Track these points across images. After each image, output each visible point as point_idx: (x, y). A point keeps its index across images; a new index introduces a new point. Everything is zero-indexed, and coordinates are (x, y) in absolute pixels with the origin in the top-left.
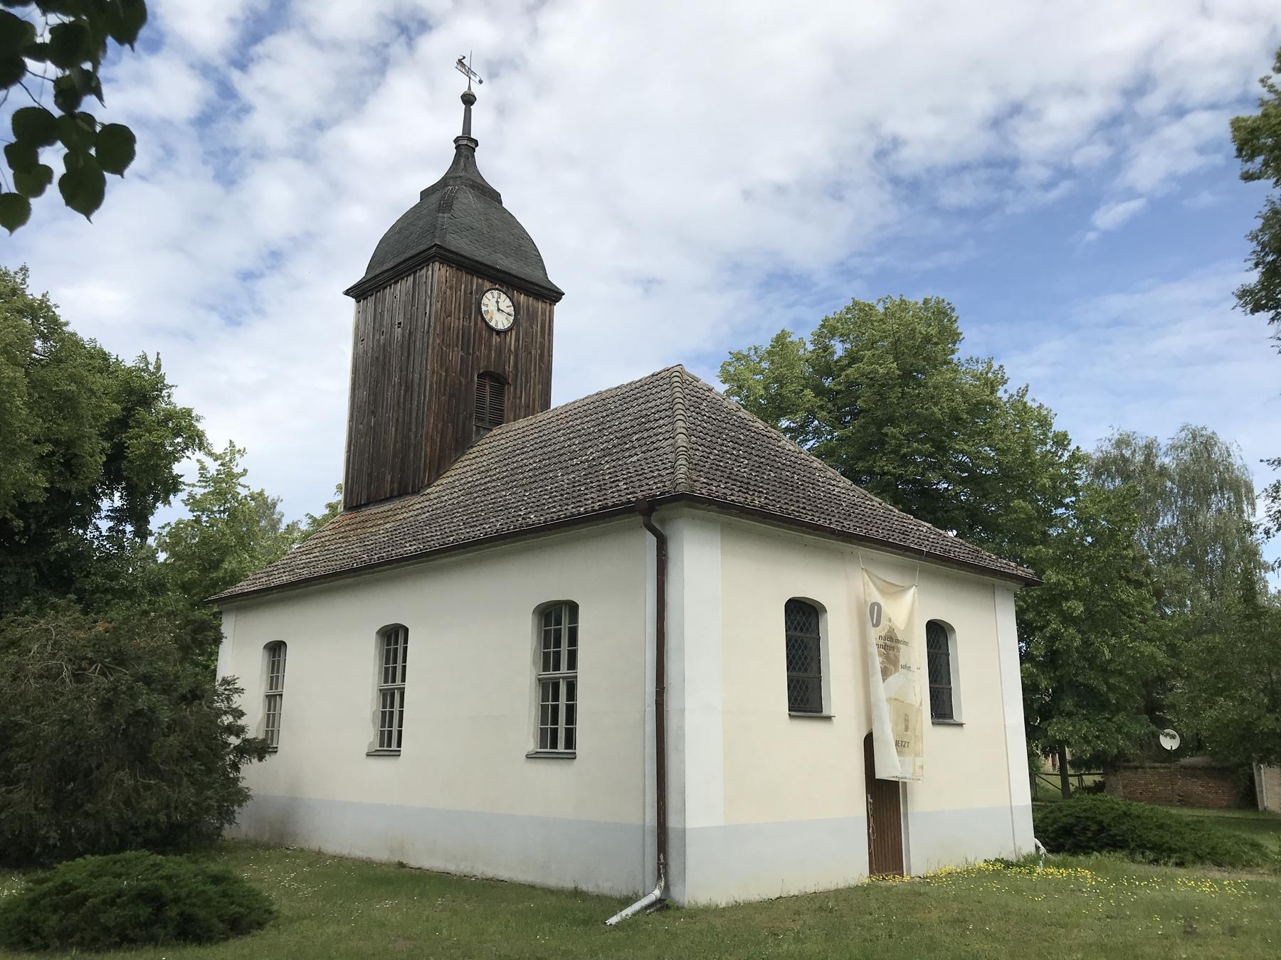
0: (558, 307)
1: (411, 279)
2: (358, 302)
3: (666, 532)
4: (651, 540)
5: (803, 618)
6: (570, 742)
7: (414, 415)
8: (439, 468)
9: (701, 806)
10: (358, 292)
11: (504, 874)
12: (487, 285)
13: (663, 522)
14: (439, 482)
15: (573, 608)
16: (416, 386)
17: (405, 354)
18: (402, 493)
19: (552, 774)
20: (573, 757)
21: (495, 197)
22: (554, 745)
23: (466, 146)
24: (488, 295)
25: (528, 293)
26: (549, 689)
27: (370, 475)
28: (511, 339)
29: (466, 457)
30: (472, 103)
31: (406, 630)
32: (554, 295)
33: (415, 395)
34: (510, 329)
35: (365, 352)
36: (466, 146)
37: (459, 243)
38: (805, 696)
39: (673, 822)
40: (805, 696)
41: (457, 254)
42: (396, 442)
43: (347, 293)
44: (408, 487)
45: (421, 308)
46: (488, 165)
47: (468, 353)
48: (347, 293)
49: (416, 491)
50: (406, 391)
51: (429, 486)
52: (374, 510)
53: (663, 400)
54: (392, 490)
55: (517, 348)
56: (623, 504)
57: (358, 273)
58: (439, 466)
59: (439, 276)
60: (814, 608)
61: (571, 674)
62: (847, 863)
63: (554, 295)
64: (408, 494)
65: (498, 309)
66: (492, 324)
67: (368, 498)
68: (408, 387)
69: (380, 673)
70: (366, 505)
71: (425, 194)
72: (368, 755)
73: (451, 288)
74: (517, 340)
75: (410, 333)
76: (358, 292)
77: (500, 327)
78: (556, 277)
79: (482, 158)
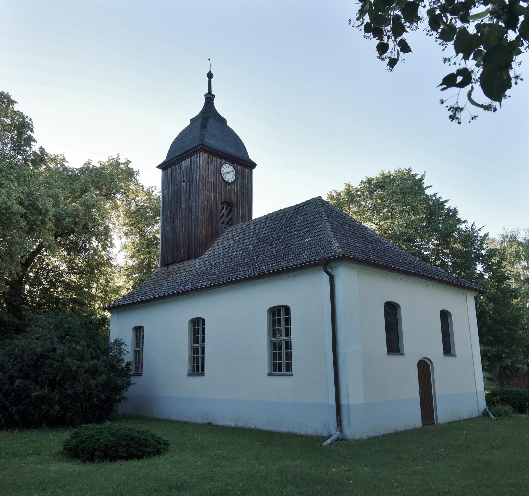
0: (254, 171)
1: (189, 160)
2: (163, 171)
3: (334, 273)
4: (327, 278)
5: (392, 311)
6: (203, 370)
7: (193, 222)
8: (206, 246)
9: (353, 395)
10: (163, 167)
11: (260, 427)
12: (224, 161)
13: (331, 268)
14: (206, 253)
15: (287, 309)
16: (194, 209)
17: (188, 194)
18: (189, 258)
19: (281, 382)
20: (203, 375)
21: (224, 121)
22: (198, 371)
23: (209, 98)
24: (224, 166)
25: (241, 165)
26: (275, 346)
27: (173, 250)
28: (234, 187)
29: (217, 241)
30: (211, 78)
31: (203, 320)
32: (253, 165)
33: (194, 213)
34: (234, 181)
35: (168, 194)
36: (209, 98)
37: (210, 142)
38: (394, 345)
39: (344, 402)
40: (394, 345)
41: (210, 148)
42: (185, 235)
43: (158, 167)
44: (193, 254)
45: (195, 173)
46: (219, 106)
47: (216, 193)
48: (158, 167)
49: (196, 257)
50: (189, 211)
51: (202, 255)
52: (176, 266)
53: (315, 213)
54: (184, 257)
55: (237, 190)
56: (312, 261)
57: (162, 158)
58: (205, 246)
59: (203, 158)
60: (395, 306)
61: (287, 338)
62: (413, 418)
63: (253, 165)
64: (192, 258)
65: (228, 173)
66: (226, 180)
67: (173, 261)
68: (190, 210)
69: (191, 339)
70: (172, 263)
71: (192, 121)
72: (188, 376)
73: (208, 164)
74: (237, 187)
75: (190, 185)
76: (163, 167)
77: (230, 181)
78: (252, 156)
79: (215, 102)
